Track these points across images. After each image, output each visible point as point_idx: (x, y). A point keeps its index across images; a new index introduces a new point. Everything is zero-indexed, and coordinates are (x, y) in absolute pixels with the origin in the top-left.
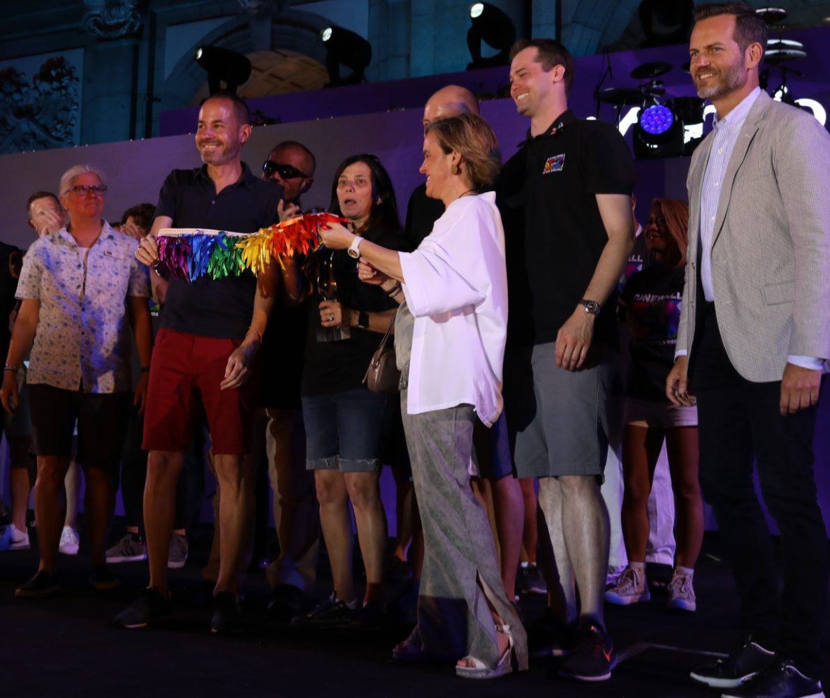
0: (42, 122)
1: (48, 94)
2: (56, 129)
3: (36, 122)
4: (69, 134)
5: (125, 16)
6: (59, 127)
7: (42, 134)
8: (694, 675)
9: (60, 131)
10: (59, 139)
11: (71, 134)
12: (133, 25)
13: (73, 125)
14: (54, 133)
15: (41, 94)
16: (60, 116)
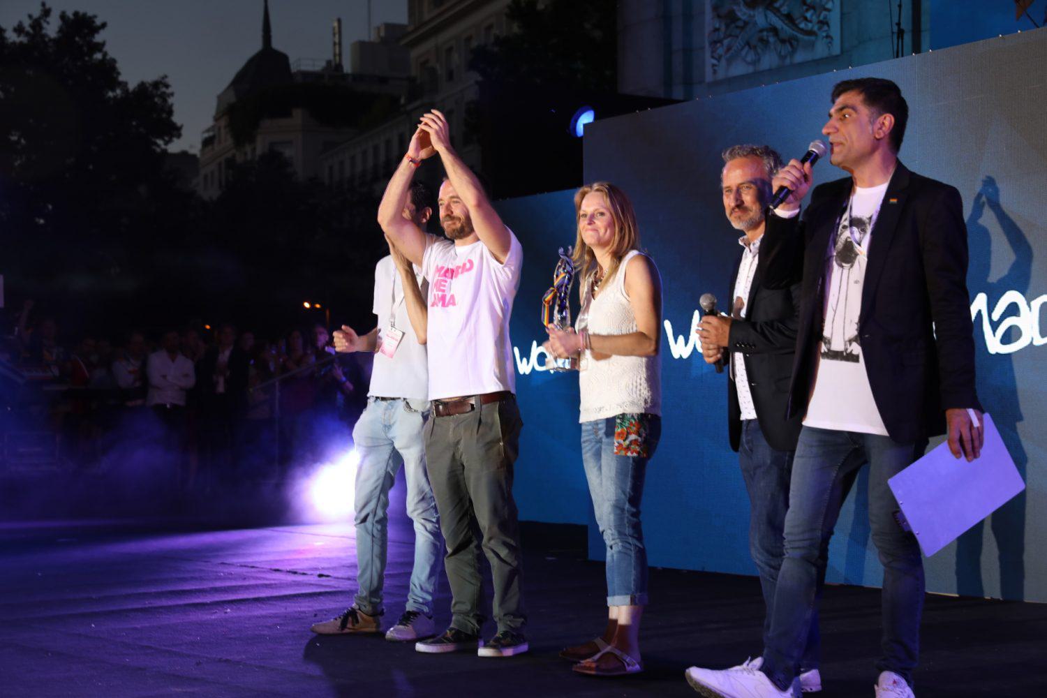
0: (785, 10)
2: (806, 19)
3: (777, 11)
4: (823, 23)
6: (808, 15)
7: (786, 28)
8: (934, 323)
9: (810, 22)
10: (810, 33)
11: (827, 24)
13: (829, 10)
14: (802, 26)
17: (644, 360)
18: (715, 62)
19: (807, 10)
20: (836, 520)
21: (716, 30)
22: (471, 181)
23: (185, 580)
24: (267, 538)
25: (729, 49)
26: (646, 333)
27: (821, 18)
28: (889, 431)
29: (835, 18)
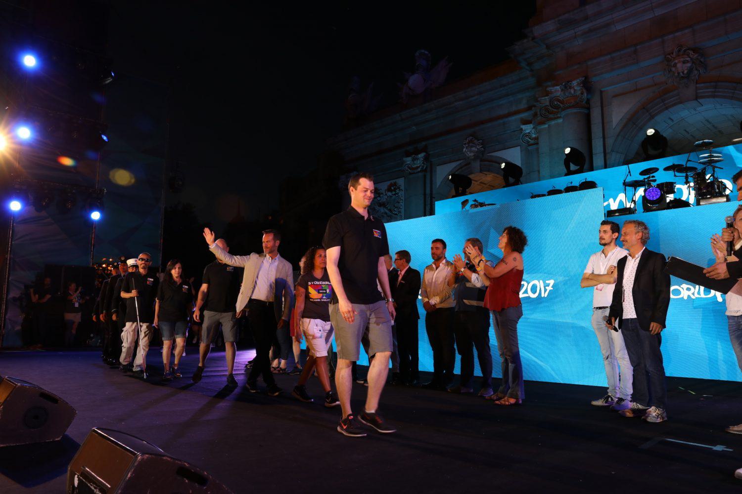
0: (389, 208)
4: (400, 212)
5: (420, 163)
6: (395, 209)
8: (208, 236)
10: (396, 214)
12: (423, 166)
16: (396, 205)
23: (218, 367)
24: (242, 354)
26: (9, 392)
28: (384, 225)
29: (403, 210)
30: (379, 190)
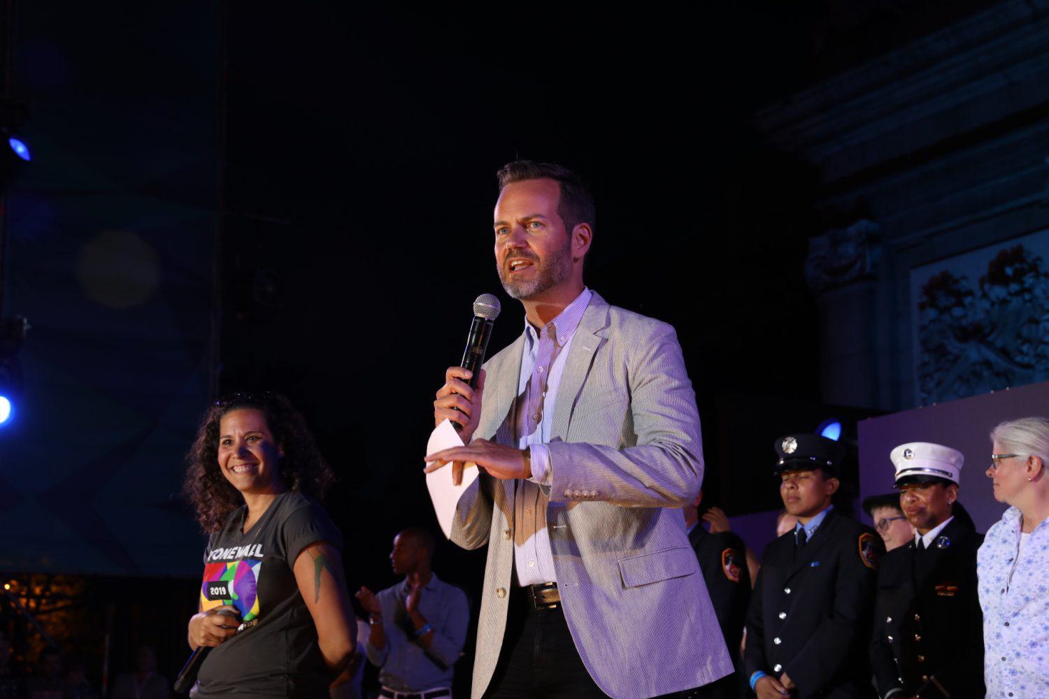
0: (999, 344)
1: (1004, 302)
2: (1021, 352)
3: (990, 345)
6: (1025, 348)
8: (947, 695)
9: (1027, 355)
10: (1028, 366)
14: (1018, 359)
15: (993, 304)
16: (1025, 332)
17: (586, 294)
18: (925, 395)
19: (1023, 344)
20: (712, 601)
21: (925, 364)
22: (1003, 423)
25: (939, 383)
27: (1039, 350)
30: (956, 281)
